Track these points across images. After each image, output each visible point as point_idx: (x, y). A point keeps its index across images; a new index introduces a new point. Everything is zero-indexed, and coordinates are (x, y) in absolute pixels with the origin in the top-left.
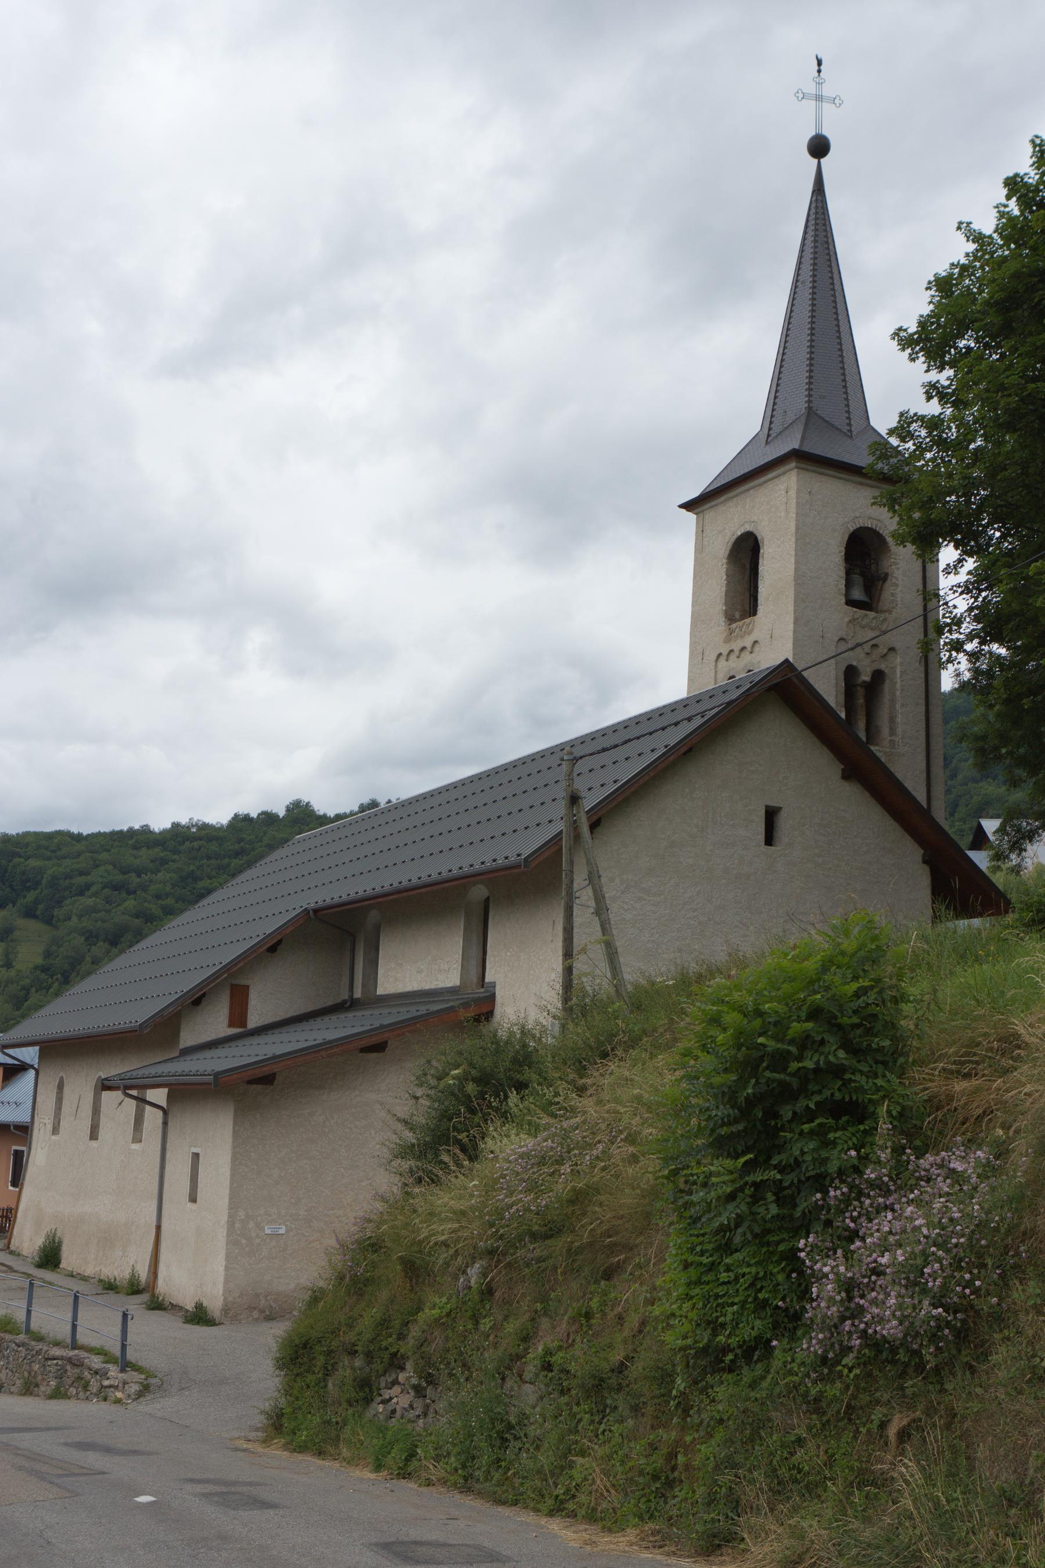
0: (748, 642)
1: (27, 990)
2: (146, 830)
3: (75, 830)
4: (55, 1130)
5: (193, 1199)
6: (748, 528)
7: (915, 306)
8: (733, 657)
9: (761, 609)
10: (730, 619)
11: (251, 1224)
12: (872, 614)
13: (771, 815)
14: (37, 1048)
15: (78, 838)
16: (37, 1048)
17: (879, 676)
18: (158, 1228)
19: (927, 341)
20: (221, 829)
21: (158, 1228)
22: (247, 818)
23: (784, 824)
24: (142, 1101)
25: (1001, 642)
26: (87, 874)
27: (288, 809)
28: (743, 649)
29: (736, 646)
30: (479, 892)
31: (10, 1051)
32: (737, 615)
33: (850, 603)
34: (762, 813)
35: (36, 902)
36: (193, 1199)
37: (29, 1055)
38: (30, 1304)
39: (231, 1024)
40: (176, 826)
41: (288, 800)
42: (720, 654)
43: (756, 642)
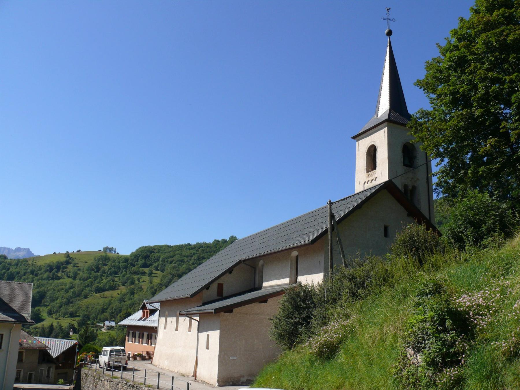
0: (374, 178)
1: (156, 290)
2: (189, 245)
3: (169, 244)
4: (165, 328)
5: (208, 348)
6: (373, 143)
7: (422, 74)
8: (369, 182)
9: (377, 167)
10: (368, 171)
11: (226, 356)
12: (411, 169)
13: (386, 228)
14: (159, 303)
15: (170, 247)
16: (159, 303)
17: (414, 188)
18: (197, 357)
19: (427, 86)
20: (210, 244)
21: (197, 357)
22: (218, 241)
23: (390, 231)
24: (191, 318)
25: (503, 132)
26: (173, 257)
27: (230, 239)
28: (372, 180)
29: (370, 179)
30: (295, 253)
31: (152, 304)
32: (370, 170)
33: (405, 165)
34: (384, 227)
35: (158, 265)
36: (208, 348)
37: (157, 305)
38: (159, 380)
39: (218, 296)
40: (198, 244)
41: (230, 236)
42: (365, 182)
43: (376, 178)
